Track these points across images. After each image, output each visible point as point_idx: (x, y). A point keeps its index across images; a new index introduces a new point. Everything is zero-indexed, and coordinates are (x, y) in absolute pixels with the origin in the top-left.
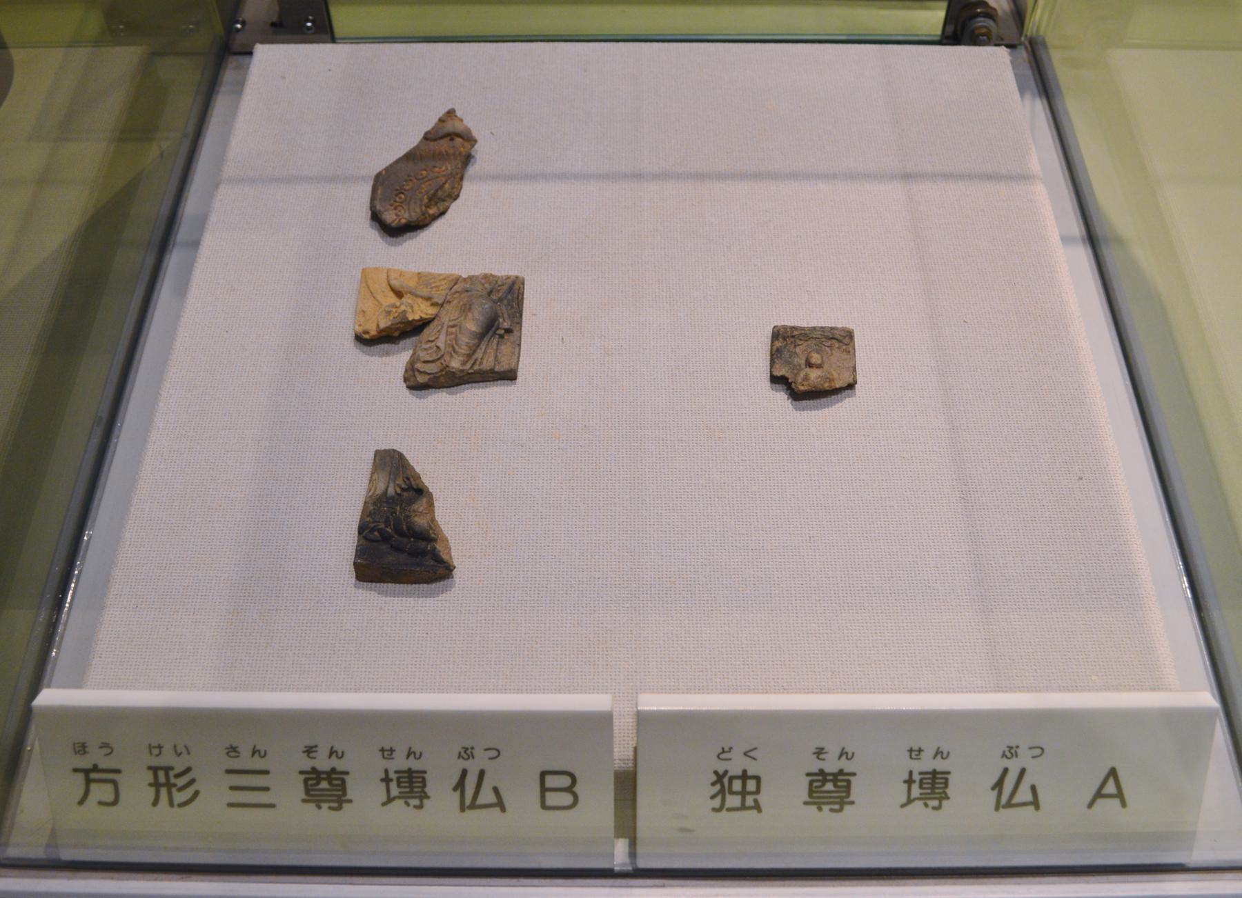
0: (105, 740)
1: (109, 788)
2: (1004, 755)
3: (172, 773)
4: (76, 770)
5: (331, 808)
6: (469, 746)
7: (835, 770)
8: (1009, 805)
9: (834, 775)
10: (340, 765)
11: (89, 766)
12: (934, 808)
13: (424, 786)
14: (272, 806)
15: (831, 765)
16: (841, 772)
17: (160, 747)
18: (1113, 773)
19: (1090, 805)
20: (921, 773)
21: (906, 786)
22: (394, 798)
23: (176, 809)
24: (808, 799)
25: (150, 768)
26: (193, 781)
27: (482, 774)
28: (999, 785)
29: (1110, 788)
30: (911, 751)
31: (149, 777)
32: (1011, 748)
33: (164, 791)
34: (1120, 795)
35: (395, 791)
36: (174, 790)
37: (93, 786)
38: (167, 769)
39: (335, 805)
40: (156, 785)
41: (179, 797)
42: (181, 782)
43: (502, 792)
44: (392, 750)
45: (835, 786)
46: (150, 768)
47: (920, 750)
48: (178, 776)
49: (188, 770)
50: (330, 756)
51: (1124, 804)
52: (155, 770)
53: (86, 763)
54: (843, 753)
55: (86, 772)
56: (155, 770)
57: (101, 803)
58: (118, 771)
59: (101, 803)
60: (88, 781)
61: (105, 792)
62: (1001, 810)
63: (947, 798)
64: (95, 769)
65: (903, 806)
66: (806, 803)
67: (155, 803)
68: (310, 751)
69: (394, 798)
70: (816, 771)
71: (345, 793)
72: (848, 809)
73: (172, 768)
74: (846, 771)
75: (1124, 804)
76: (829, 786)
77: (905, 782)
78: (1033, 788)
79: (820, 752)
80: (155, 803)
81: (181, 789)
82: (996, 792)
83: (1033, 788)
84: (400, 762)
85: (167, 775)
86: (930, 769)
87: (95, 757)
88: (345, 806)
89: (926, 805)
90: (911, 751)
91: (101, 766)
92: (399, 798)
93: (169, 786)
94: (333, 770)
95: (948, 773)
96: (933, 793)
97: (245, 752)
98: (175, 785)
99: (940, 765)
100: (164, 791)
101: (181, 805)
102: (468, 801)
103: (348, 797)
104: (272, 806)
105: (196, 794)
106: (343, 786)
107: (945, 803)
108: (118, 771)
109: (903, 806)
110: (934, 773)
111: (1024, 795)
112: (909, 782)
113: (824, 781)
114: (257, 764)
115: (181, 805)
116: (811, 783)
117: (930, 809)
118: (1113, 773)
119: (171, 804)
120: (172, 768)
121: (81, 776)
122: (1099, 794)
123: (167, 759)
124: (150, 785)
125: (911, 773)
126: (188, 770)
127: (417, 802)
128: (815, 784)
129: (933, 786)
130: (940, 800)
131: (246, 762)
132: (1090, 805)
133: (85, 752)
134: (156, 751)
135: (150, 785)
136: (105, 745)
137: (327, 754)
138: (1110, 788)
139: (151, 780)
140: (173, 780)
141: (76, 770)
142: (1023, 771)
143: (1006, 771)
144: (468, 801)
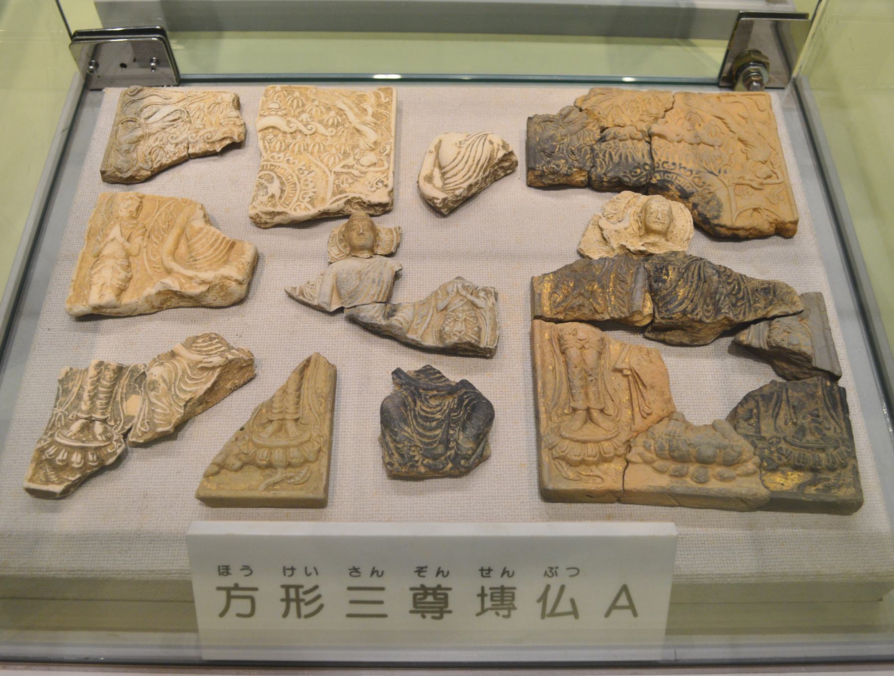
0: (246, 564)
1: (248, 602)
2: (546, 574)
3: (301, 591)
4: (219, 589)
5: (434, 618)
6: (554, 566)
7: (434, 585)
8: (553, 614)
9: (434, 589)
10: (444, 582)
11: (232, 585)
12: (504, 616)
13: (513, 599)
14: (385, 616)
15: (431, 581)
16: (439, 587)
17: (293, 569)
18: (625, 589)
19: (607, 615)
20: (491, 589)
21: (479, 598)
22: (487, 609)
23: (303, 618)
24: (413, 609)
25: (283, 586)
26: (319, 597)
27: (563, 588)
28: (543, 598)
29: (623, 601)
30: (482, 570)
31: (282, 593)
32: (552, 568)
33: (293, 605)
34: (631, 607)
35: (488, 603)
36: (302, 604)
37: (234, 602)
38: (297, 588)
39: (438, 615)
40: (287, 600)
41: (305, 610)
42: (308, 597)
43: (578, 604)
44: (490, 570)
45: (435, 598)
46: (283, 586)
47: (490, 570)
48: (305, 593)
49: (316, 587)
50: (437, 575)
51: (635, 614)
52: (287, 588)
53: (228, 582)
54: (439, 572)
55: (228, 590)
56: (287, 588)
57: (239, 615)
58: (256, 589)
59: (239, 615)
60: (229, 598)
61: (244, 606)
62: (546, 618)
63: (515, 609)
64: (236, 587)
65: (478, 615)
66: (411, 612)
67: (285, 615)
68: (420, 571)
69: (487, 609)
70: (419, 586)
71: (447, 606)
72: (446, 616)
73: (302, 587)
74: (443, 586)
75: (635, 614)
76: (430, 599)
77: (478, 595)
78: (572, 601)
79: (420, 571)
80: (285, 615)
81: (307, 604)
82: (541, 604)
83: (572, 601)
84: (496, 580)
85: (297, 593)
86: (499, 586)
87: (236, 578)
88: (446, 616)
89: (497, 614)
90: (482, 570)
91: (241, 585)
92: (491, 609)
93: (298, 600)
94: (439, 587)
95: (515, 588)
96: (502, 604)
97: (366, 570)
98: (303, 600)
99: (507, 582)
100: (293, 605)
101: (307, 616)
102: (549, 609)
103: (449, 609)
104: (385, 616)
105: (321, 606)
106: (415, 602)
107: (513, 612)
108: (256, 589)
109: (478, 615)
110: (502, 588)
111: (565, 606)
112: (482, 595)
113: (426, 595)
114: (375, 582)
115: (307, 616)
116: (415, 595)
117: (500, 617)
118: (625, 589)
119: (299, 616)
120: (302, 587)
121: (224, 594)
122: (613, 606)
123: (298, 579)
124: (282, 600)
125: (483, 588)
126: (316, 587)
127: (505, 612)
128: (419, 597)
129: (502, 599)
130: (509, 610)
131: (365, 580)
132: (607, 615)
133: (228, 574)
134: (289, 572)
135: (282, 600)
136: (246, 568)
137: (501, 571)
138: (623, 601)
139: (283, 596)
140: (302, 596)
141: (219, 589)
142: (563, 588)
143: (548, 587)
144: (549, 609)
